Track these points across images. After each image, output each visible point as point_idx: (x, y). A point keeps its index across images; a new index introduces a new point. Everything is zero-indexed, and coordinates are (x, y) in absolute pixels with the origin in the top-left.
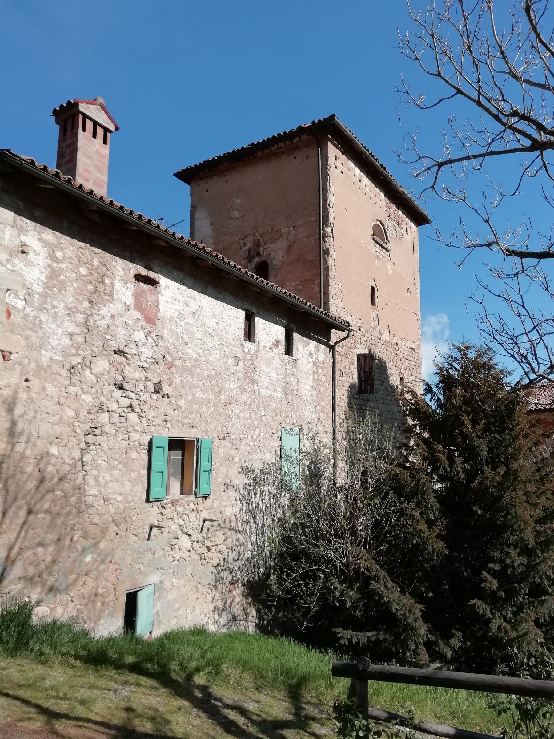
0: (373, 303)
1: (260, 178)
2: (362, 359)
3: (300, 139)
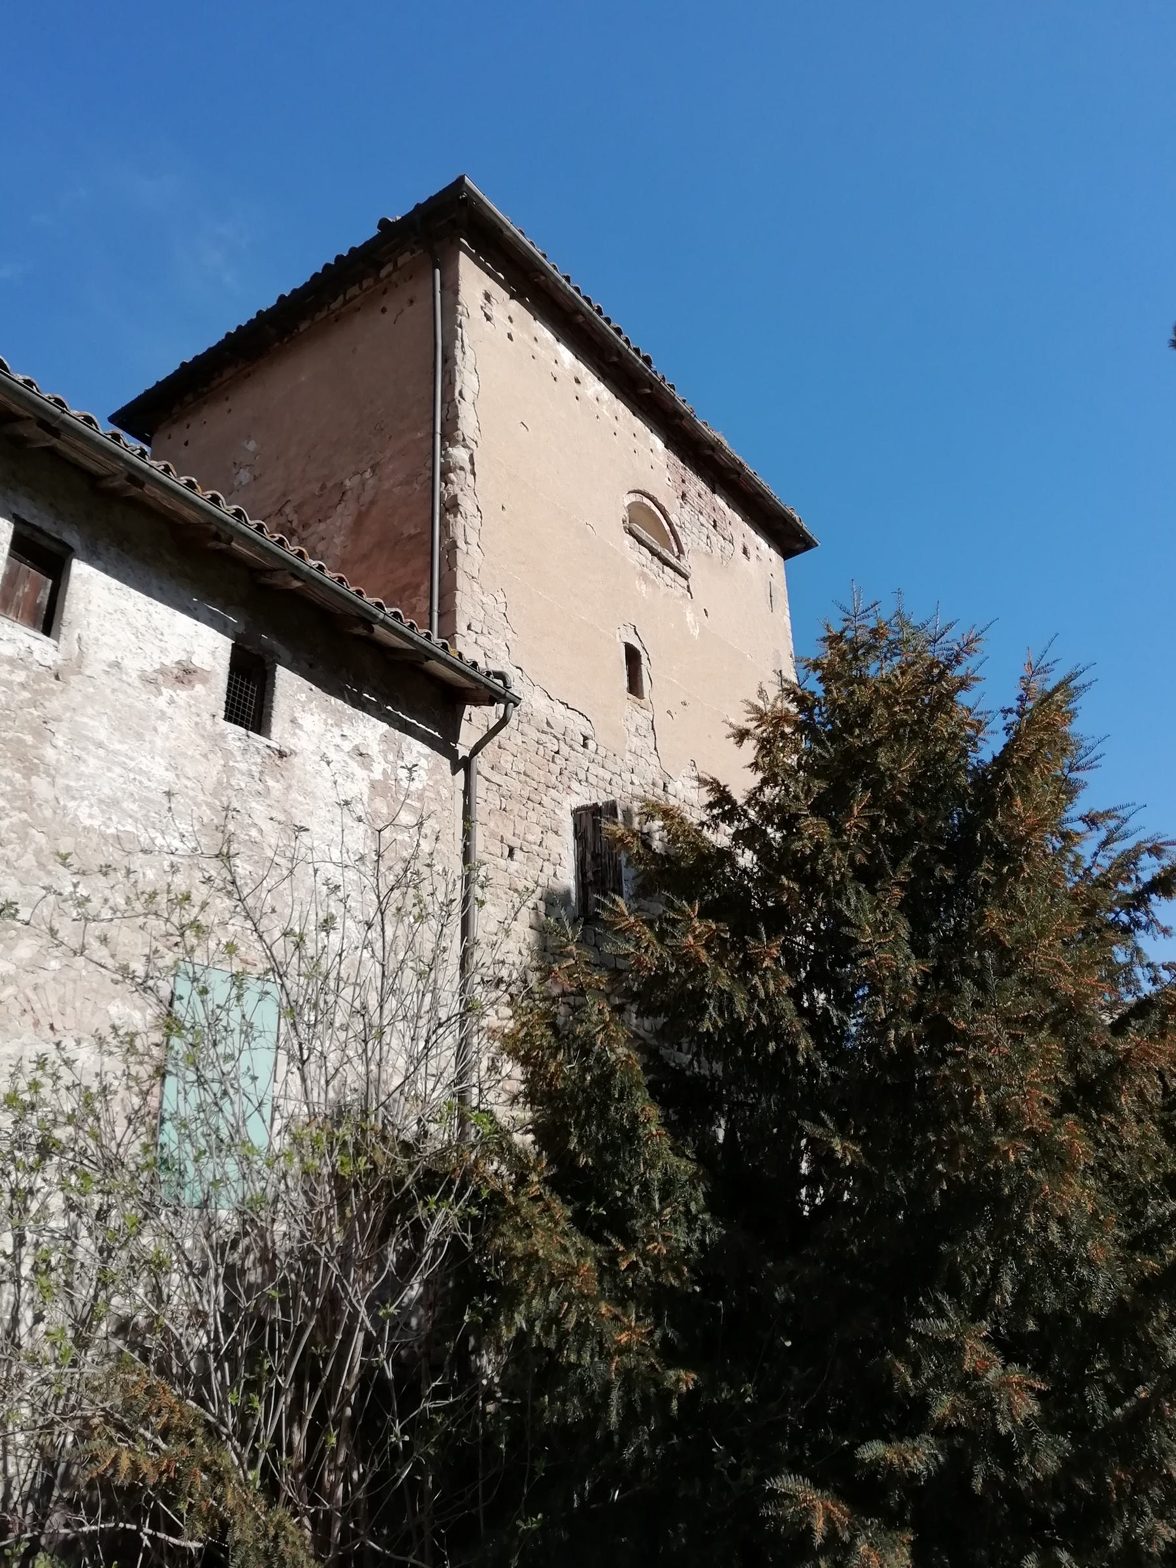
0: (635, 686)
1: (303, 379)
2: (587, 822)
3: (395, 265)
